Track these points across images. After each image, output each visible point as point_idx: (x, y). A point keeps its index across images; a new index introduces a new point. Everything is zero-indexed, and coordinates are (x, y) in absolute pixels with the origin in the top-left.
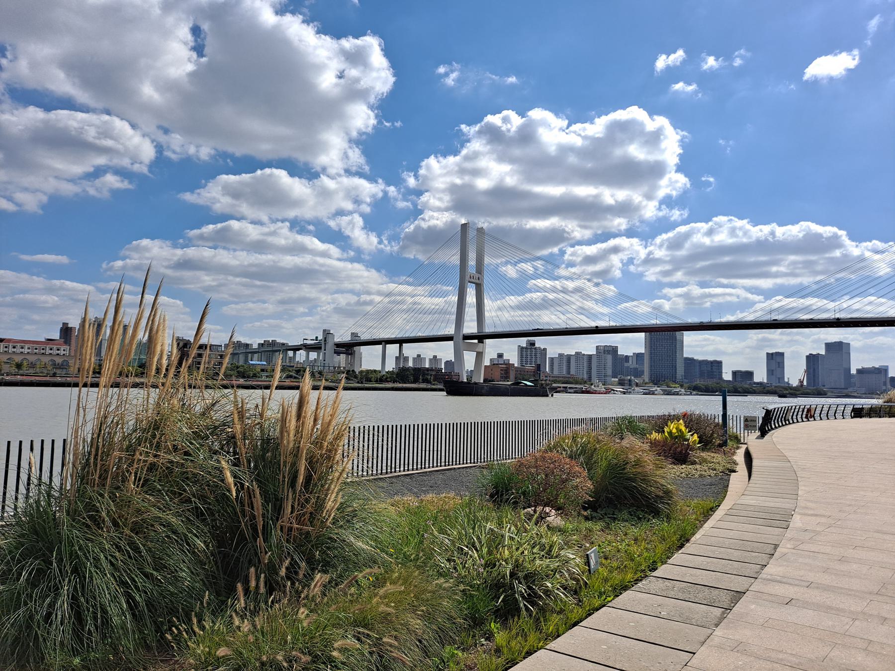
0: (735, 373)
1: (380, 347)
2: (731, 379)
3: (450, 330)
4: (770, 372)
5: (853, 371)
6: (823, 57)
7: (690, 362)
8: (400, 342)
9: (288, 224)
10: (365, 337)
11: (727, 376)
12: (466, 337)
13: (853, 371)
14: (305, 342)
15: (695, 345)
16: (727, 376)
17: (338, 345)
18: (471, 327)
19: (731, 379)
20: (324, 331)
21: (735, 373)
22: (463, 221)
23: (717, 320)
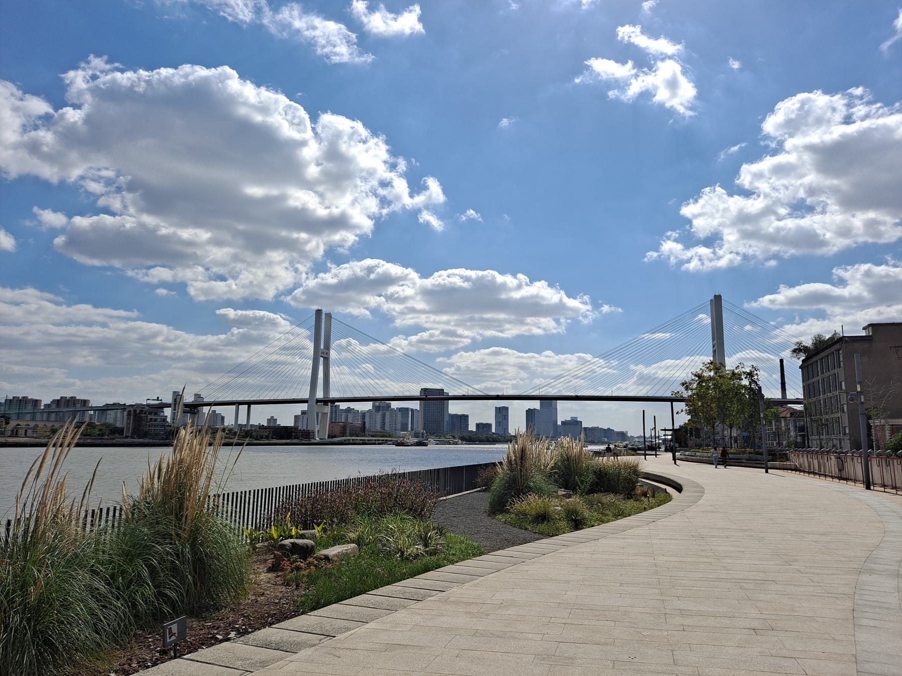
0: (478, 425)
1: (234, 407)
2: (474, 430)
3: (306, 395)
4: (498, 423)
5: (559, 423)
6: (612, 62)
7: (450, 415)
8: (249, 404)
9: (870, 421)
10: (206, 400)
11: (472, 427)
12: (318, 401)
13: (559, 423)
14: (149, 402)
15: (565, 412)
16: (472, 427)
17: (186, 405)
18: (320, 394)
19: (474, 430)
20: (174, 392)
21: (478, 425)
22: (316, 307)
23: (580, 394)
